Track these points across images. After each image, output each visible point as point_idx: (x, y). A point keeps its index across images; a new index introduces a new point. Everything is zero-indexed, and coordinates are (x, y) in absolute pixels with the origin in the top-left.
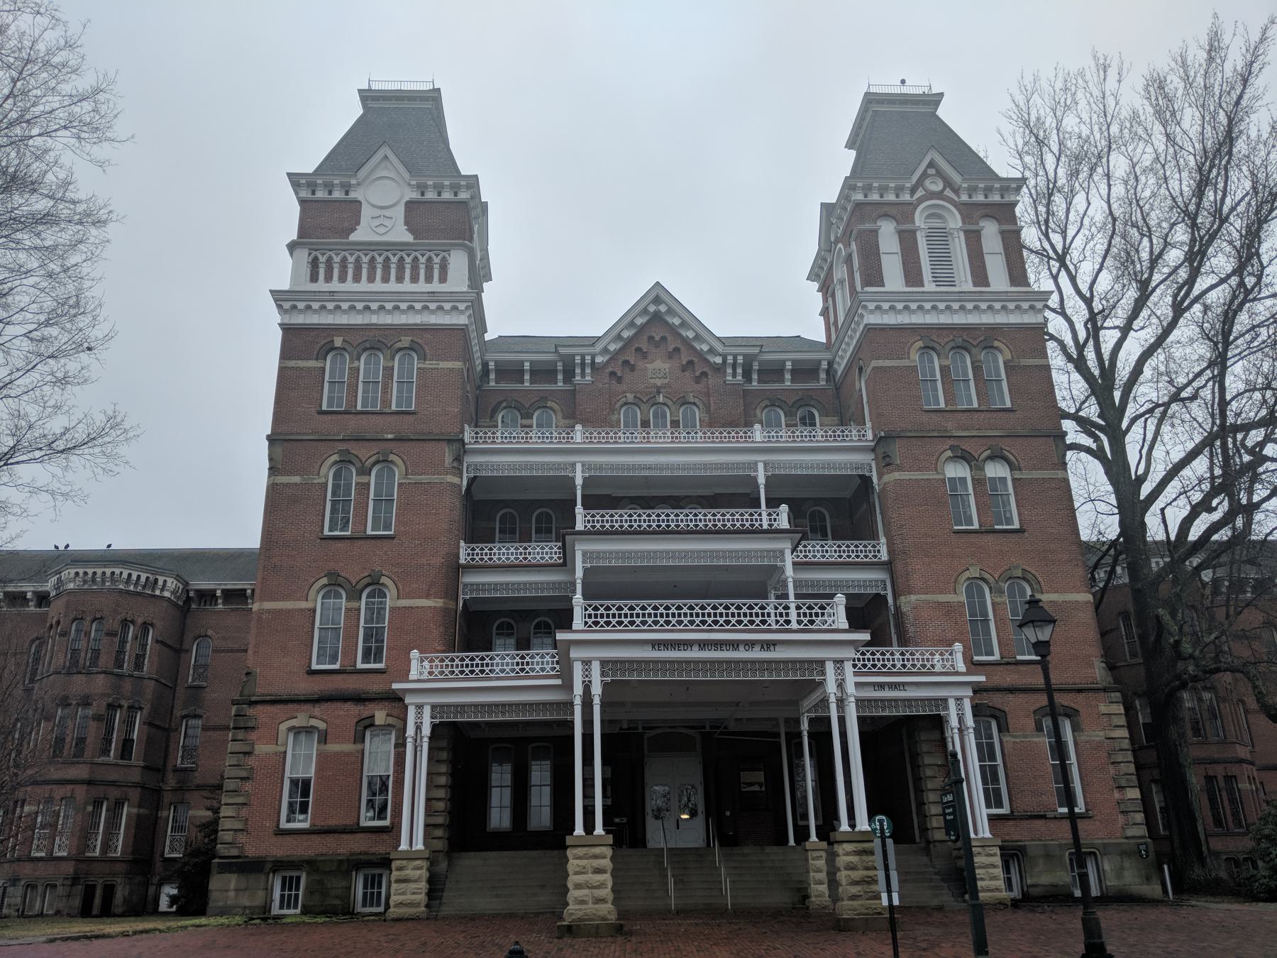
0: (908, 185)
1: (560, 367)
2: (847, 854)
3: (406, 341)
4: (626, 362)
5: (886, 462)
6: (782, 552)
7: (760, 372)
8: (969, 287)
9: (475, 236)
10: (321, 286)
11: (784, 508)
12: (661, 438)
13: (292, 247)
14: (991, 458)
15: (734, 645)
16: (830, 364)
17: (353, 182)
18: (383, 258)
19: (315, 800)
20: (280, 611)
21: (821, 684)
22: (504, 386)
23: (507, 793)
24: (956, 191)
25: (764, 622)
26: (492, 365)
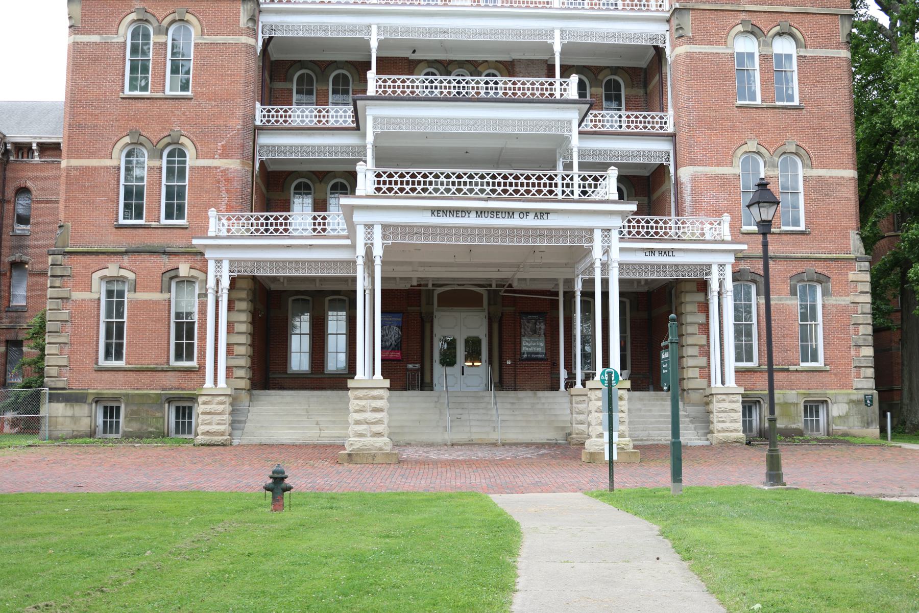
6: (570, 122)
11: (574, 79)
15: (510, 213)
19: (128, 342)
21: (589, 251)
23: (306, 340)
25: (551, 192)
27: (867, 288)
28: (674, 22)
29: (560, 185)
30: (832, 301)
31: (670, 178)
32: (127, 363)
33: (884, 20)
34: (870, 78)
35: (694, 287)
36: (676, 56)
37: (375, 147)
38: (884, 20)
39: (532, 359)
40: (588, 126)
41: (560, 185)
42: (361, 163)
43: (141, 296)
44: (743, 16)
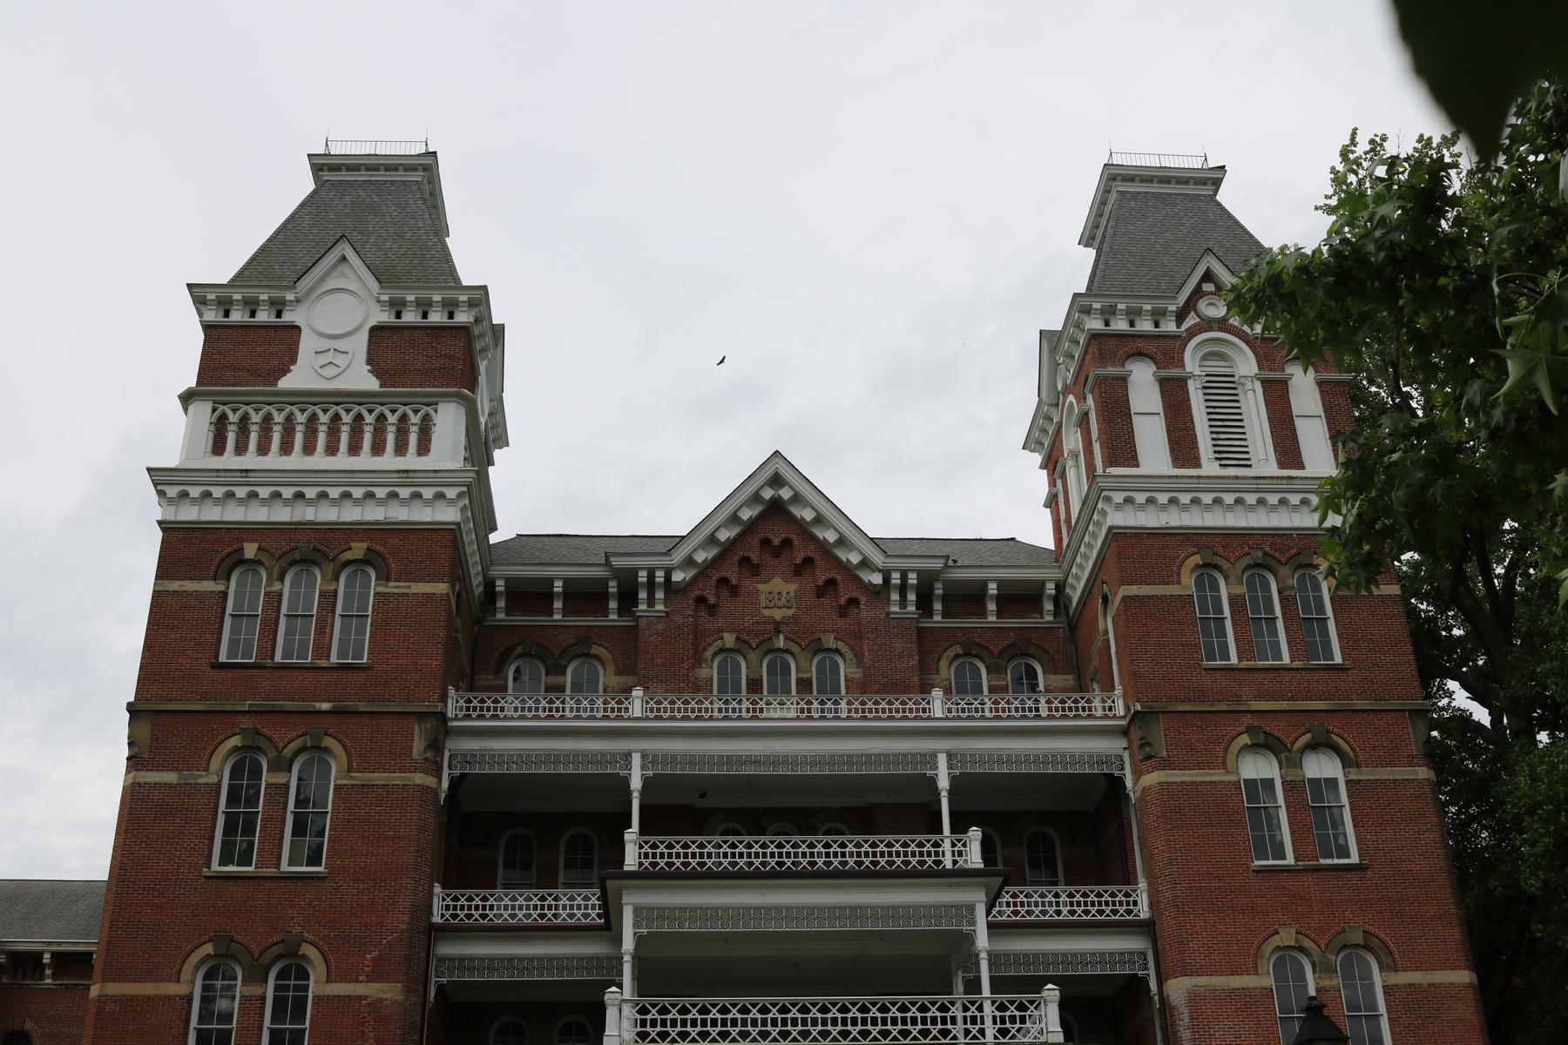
0: (1172, 308)
1: (613, 587)
3: (358, 549)
4: (723, 581)
5: (1146, 758)
6: (971, 908)
7: (945, 599)
8: (1272, 469)
9: (482, 379)
10: (229, 460)
11: (975, 834)
12: (783, 711)
13: (187, 398)
14: (1313, 747)
16: (1060, 587)
17: (290, 296)
18: (332, 417)
20: (134, 999)
22: (519, 619)
26: (500, 586)
28: (1136, 734)
29: (960, 1020)
31: (1151, 999)
33: (1481, 715)
34: (1473, 810)
36: (1144, 789)
37: (637, 957)
38: (1481, 715)
40: (1004, 913)
41: (960, 1020)
42: (614, 989)
44: (1248, 720)
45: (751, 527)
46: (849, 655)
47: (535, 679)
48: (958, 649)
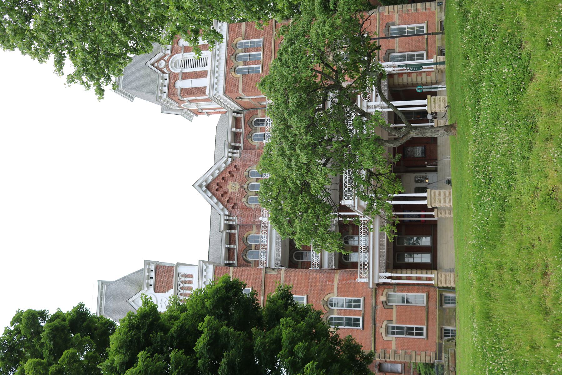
2: (435, 107)
4: (228, 201)
16: (234, 112)
24: (166, 55)
26: (227, 262)
27: (391, 7)
30: (397, 21)
32: (424, 325)
35: (391, 80)
39: (425, 152)
43: (394, 318)
45: (213, 194)
46: (250, 168)
47: (252, 253)
48: (249, 140)
